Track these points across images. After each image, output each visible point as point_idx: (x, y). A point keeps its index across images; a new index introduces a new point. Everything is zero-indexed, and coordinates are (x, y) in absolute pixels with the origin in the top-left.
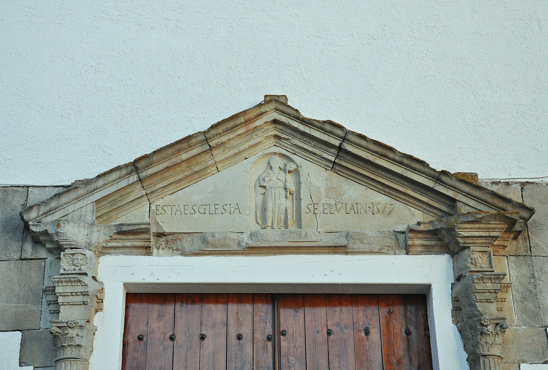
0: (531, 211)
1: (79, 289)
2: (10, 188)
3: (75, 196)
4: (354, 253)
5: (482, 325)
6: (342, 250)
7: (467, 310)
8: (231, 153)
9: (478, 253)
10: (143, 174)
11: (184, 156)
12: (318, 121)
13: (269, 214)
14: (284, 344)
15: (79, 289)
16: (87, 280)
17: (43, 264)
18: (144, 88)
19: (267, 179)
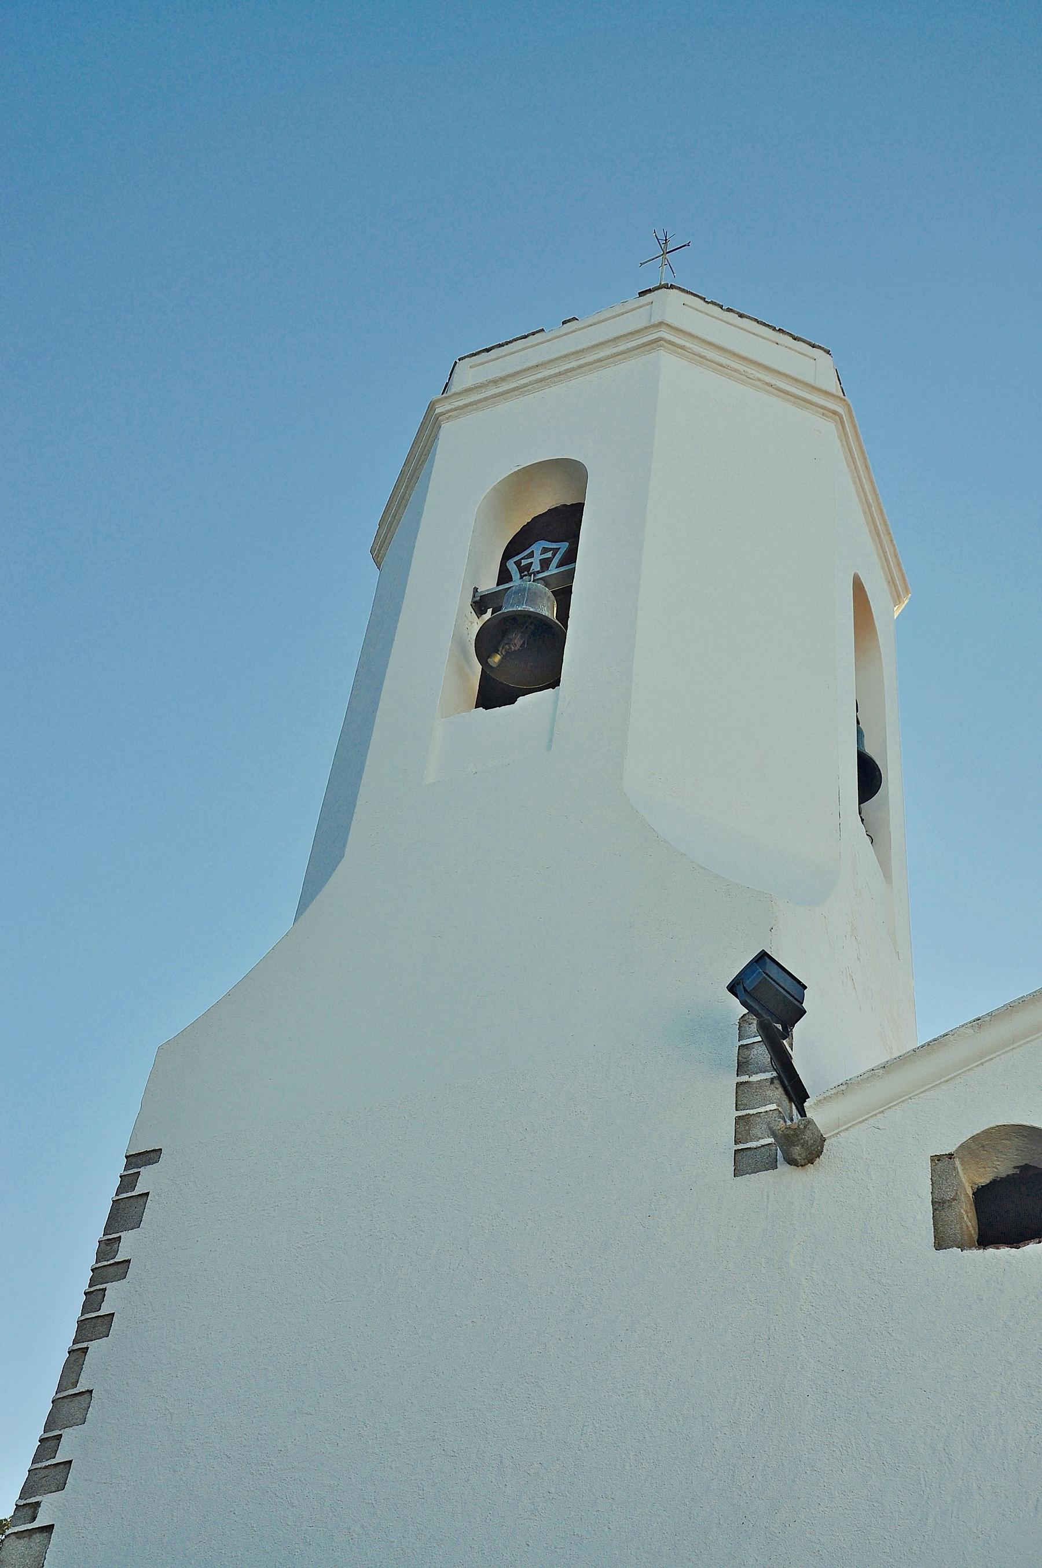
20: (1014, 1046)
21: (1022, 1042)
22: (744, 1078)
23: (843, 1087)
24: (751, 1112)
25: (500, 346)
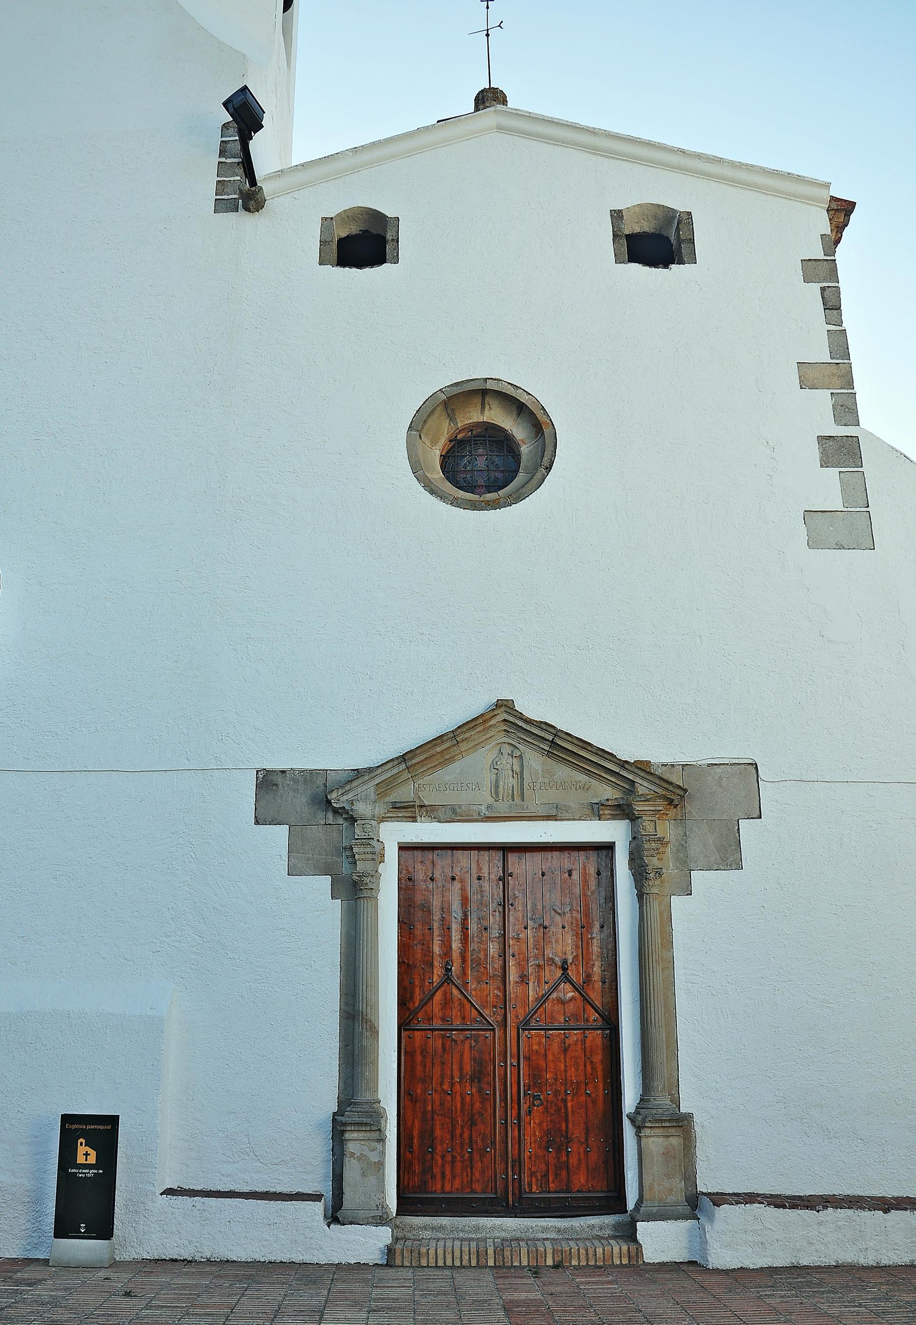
0: (685, 791)
1: (369, 850)
2: (314, 771)
3: (362, 781)
4: (561, 820)
5: (647, 873)
6: (553, 818)
7: (638, 861)
8: (472, 744)
9: (647, 822)
10: (410, 763)
11: (438, 749)
12: (537, 721)
13: (501, 790)
14: (511, 882)
15: (369, 850)
16: (374, 843)
17: (341, 828)
18: (406, 691)
19: (498, 763)
20: (372, 166)
21: (376, 165)
22: (223, 160)
23: (280, 173)
24: (226, 179)
25: (867, 497)
